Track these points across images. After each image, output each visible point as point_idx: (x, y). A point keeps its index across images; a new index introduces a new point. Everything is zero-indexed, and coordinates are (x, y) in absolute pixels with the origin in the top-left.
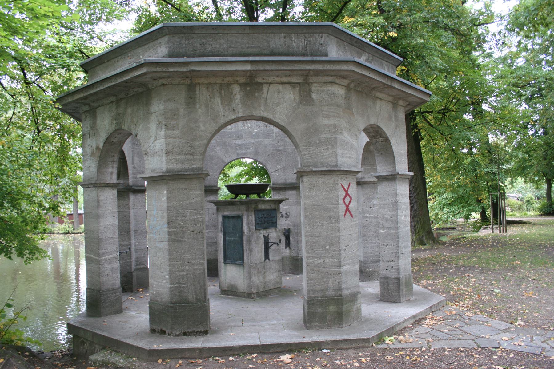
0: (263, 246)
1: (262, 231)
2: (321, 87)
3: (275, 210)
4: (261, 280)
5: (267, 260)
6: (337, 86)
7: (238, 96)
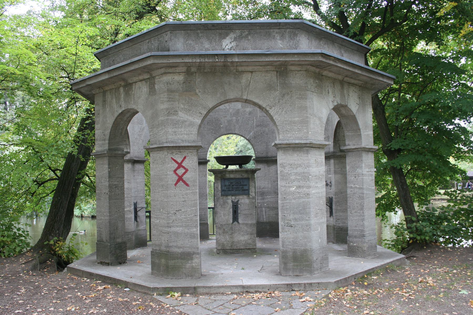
0: (231, 210)
1: (229, 197)
2: (160, 78)
3: (248, 179)
4: (228, 239)
5: (236, 223)
6: (169, 74)
7: (122, 96)
